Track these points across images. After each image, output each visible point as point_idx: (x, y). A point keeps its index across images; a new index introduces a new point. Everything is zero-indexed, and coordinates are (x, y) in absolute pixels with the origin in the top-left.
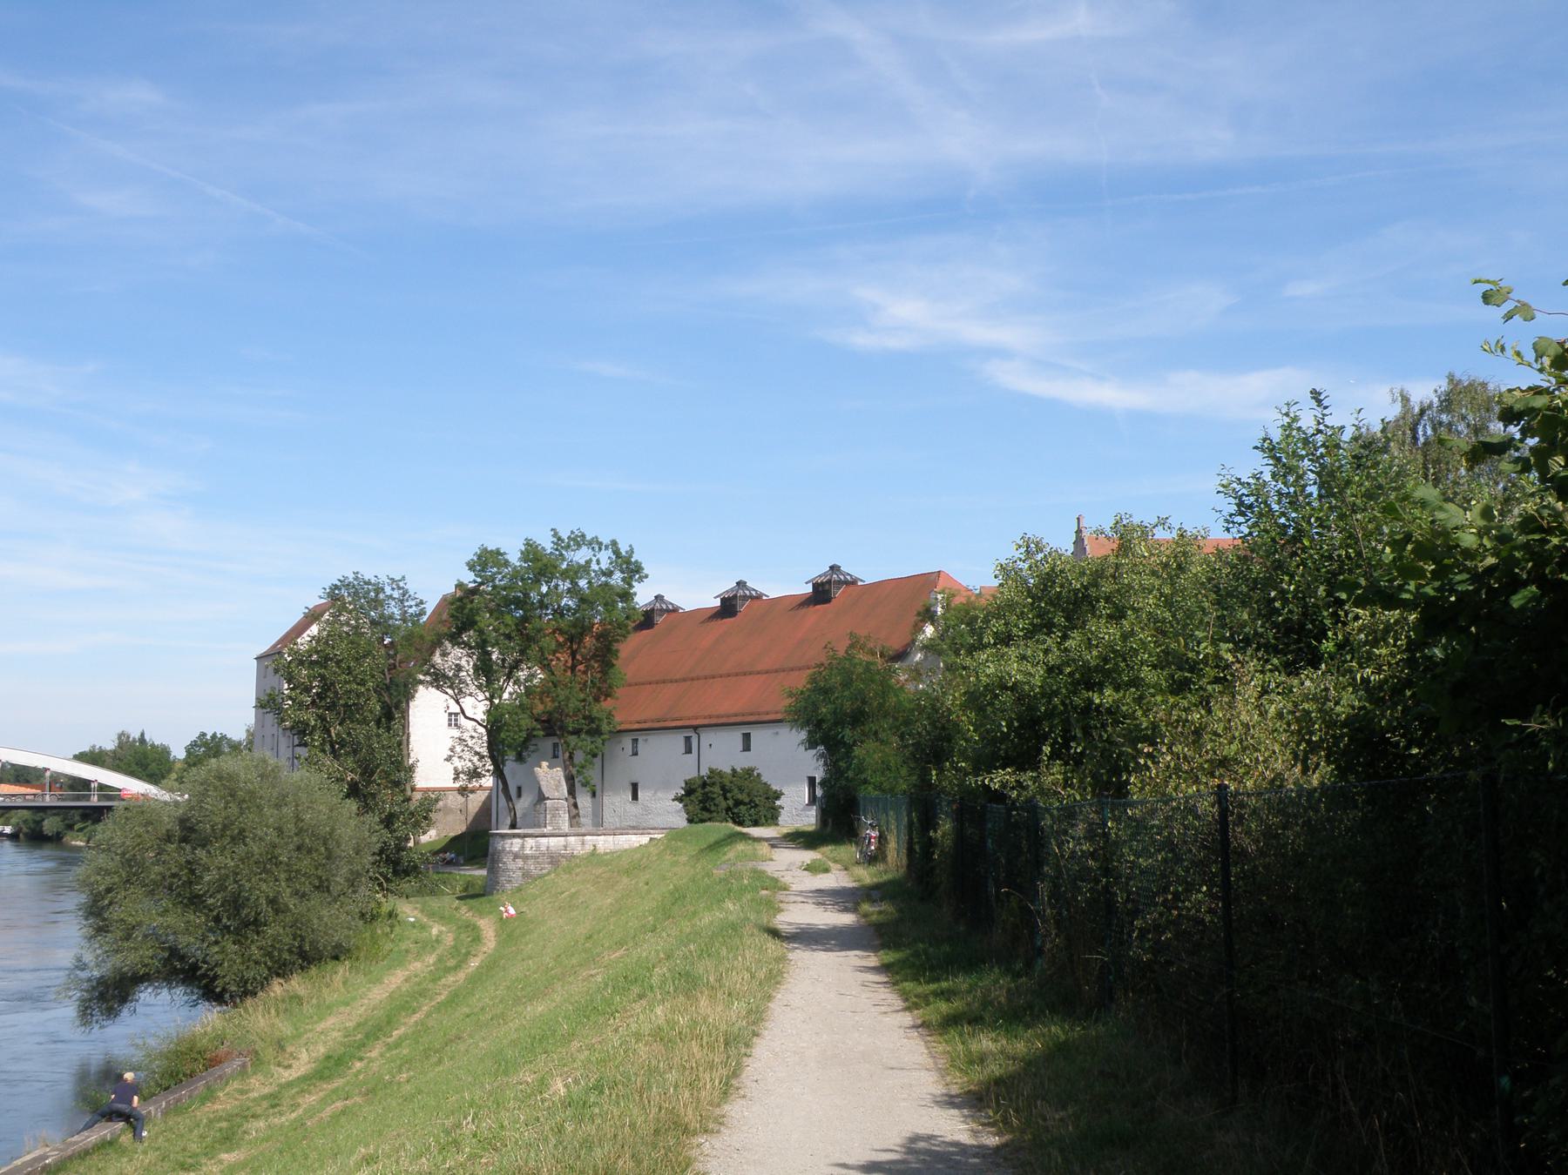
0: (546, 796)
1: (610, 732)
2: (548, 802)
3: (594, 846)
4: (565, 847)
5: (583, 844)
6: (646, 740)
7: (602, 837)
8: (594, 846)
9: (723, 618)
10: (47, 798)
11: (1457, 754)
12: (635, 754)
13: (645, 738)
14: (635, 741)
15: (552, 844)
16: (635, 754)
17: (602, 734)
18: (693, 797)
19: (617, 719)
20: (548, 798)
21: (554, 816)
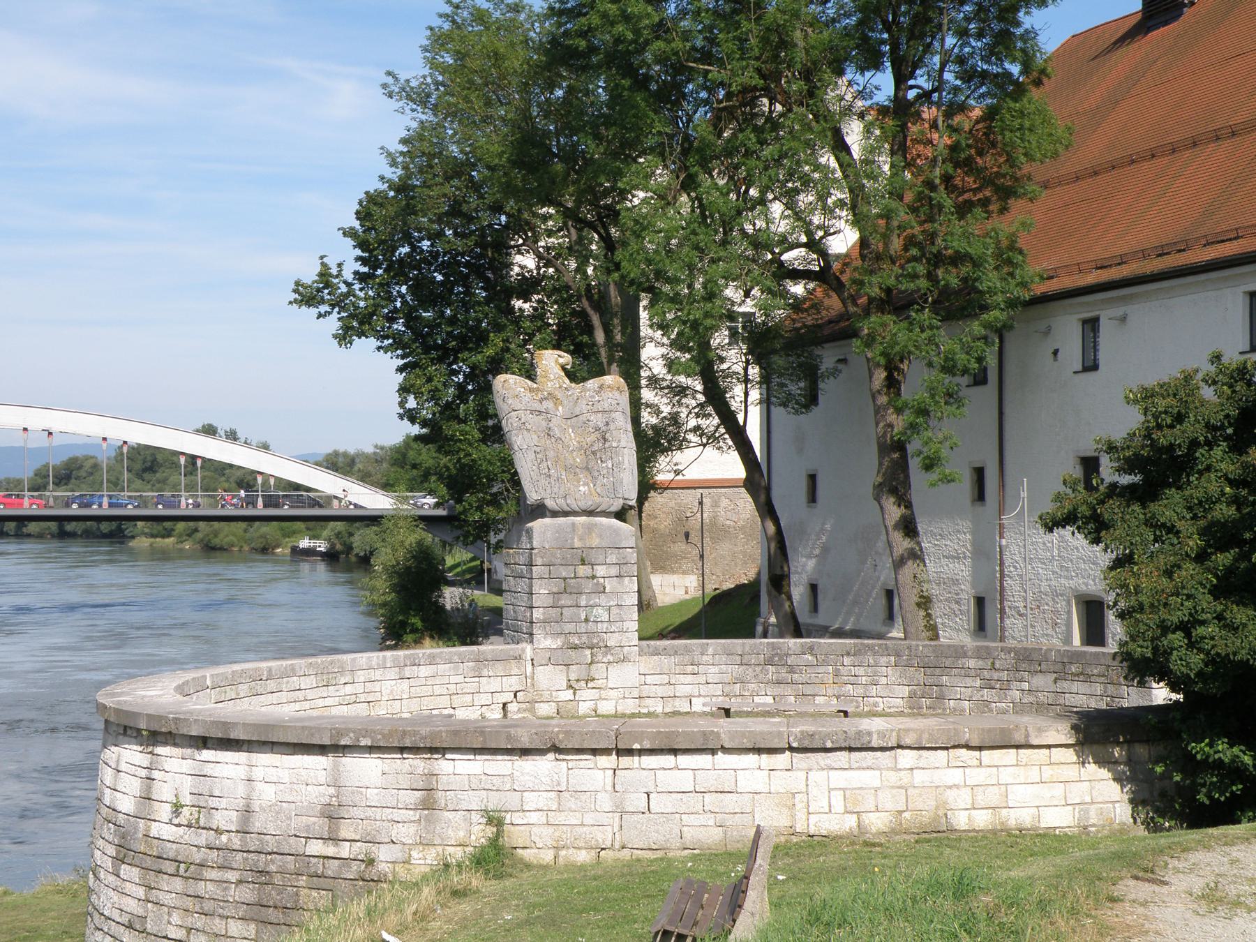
0: (532, 495)
1: (1012, 304)
2: (538, 525)
3: (495, 820)
4: (332, 814)
5: (428, 804)
6: (1123, 319)
7: (544, 766)
8: (495, 820)
9: (1146, 33)
10: (26, 502)
11: (1240, 787)
12: (1091, 366)
13: (1119, 311)
14: (1091, 325)
15: (266, 794)
16: (1091, 366)
17: (985, 308)
18: (1170, 507)
19: (1031, 268)
20: (540, 510)
21: (567, 588)
